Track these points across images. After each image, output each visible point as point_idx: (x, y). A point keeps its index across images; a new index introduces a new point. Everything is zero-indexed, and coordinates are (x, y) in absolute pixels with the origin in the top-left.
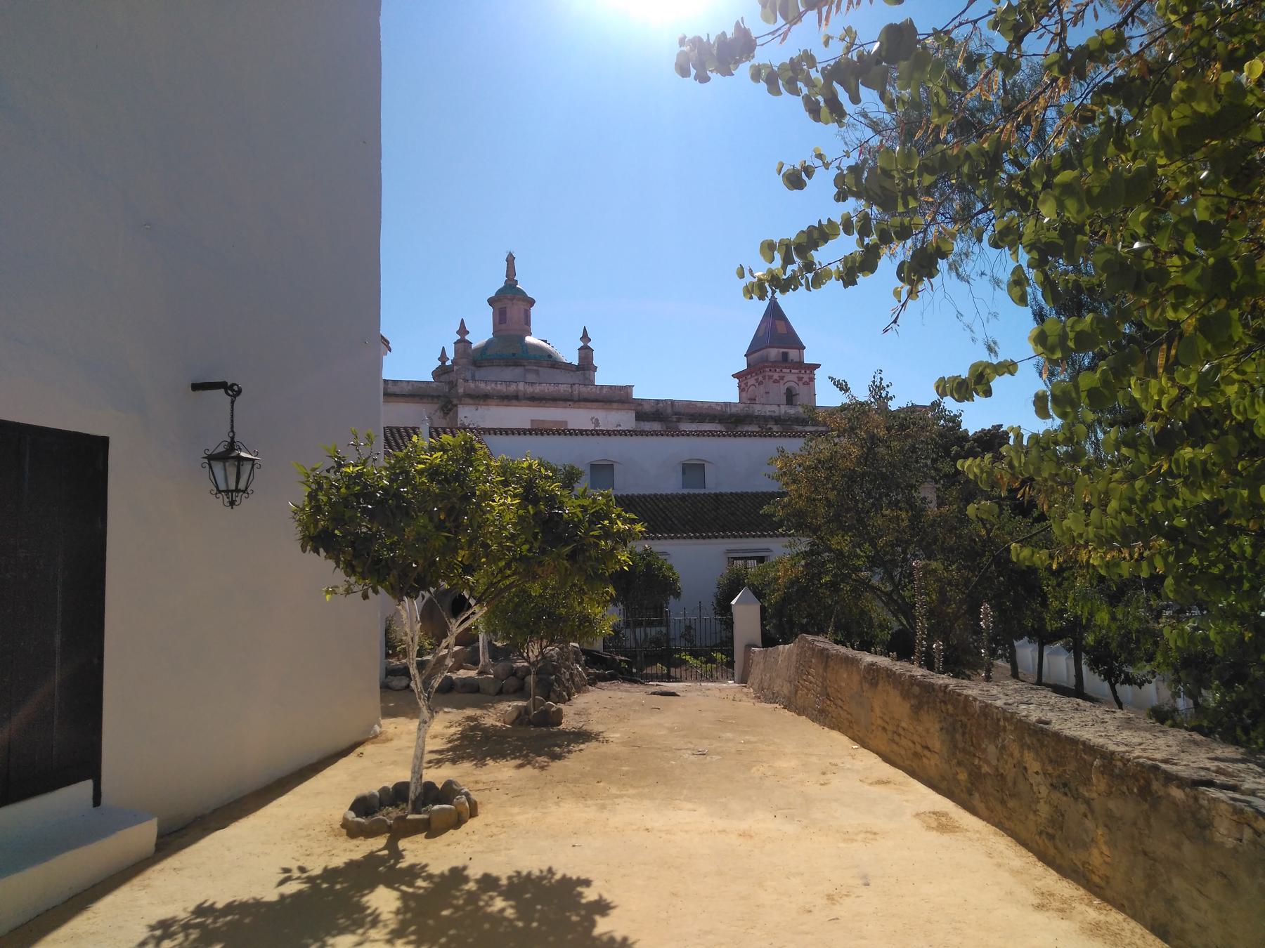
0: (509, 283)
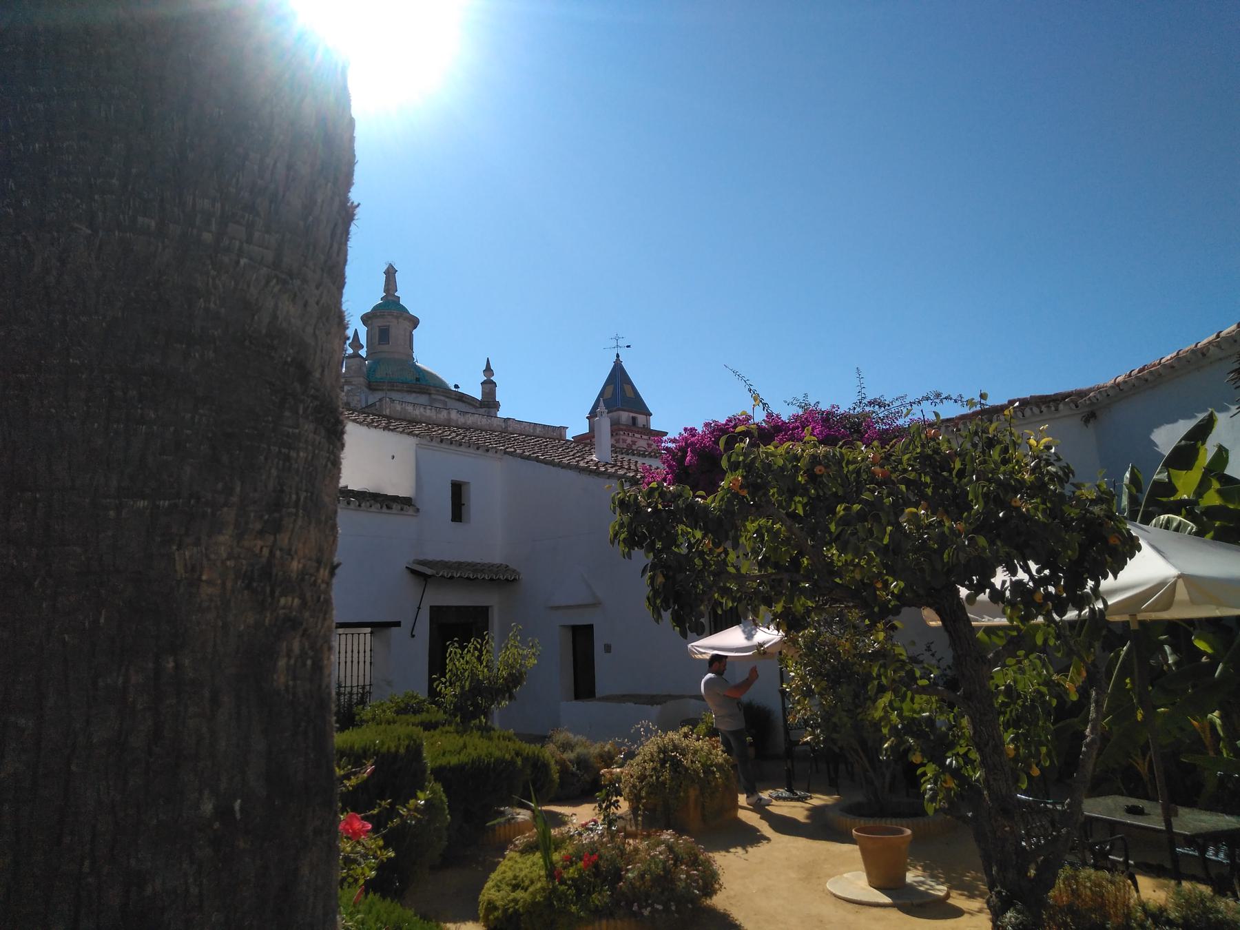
0: (390, 298)
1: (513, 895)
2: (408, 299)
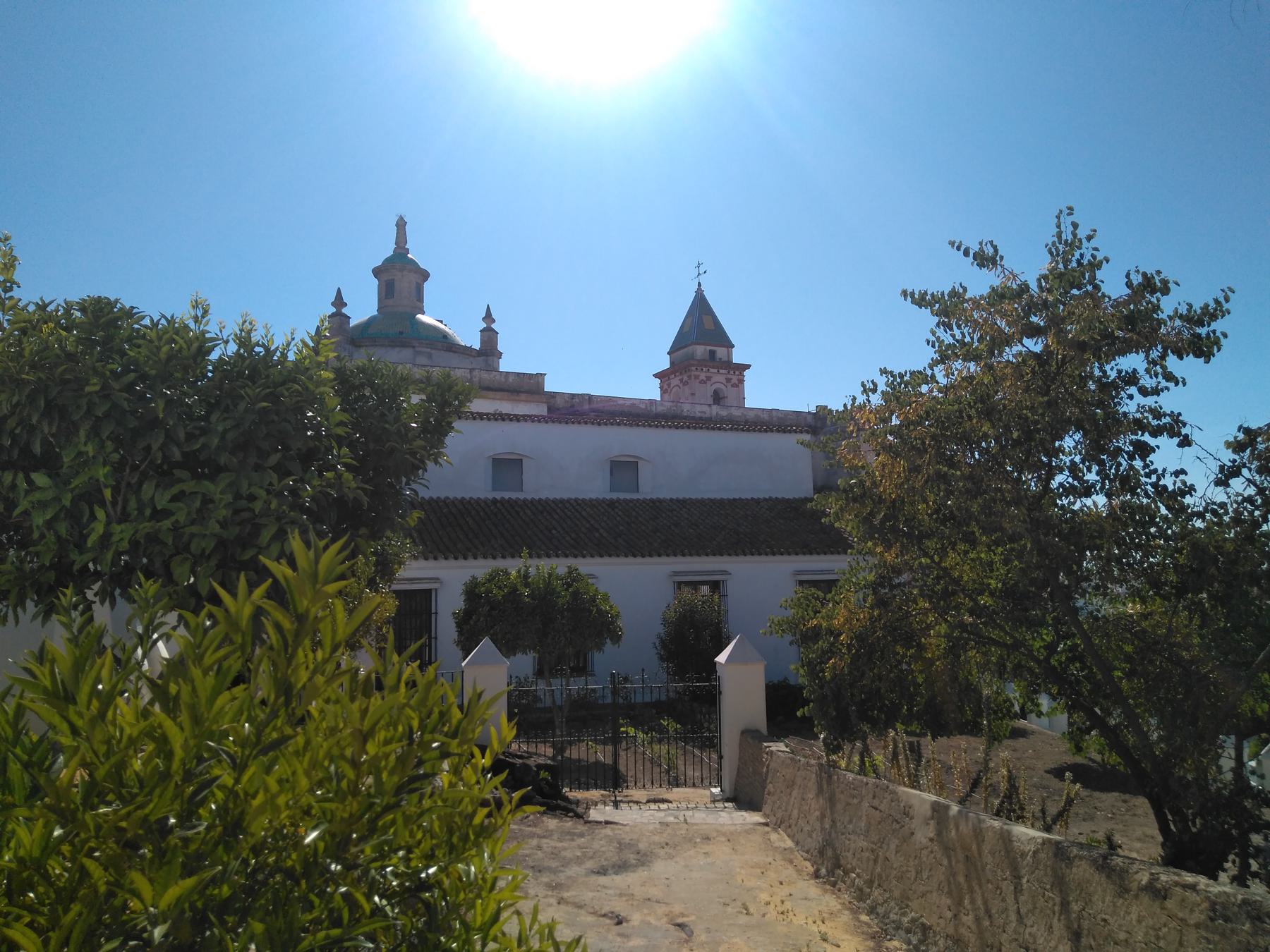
0: (400, 251)
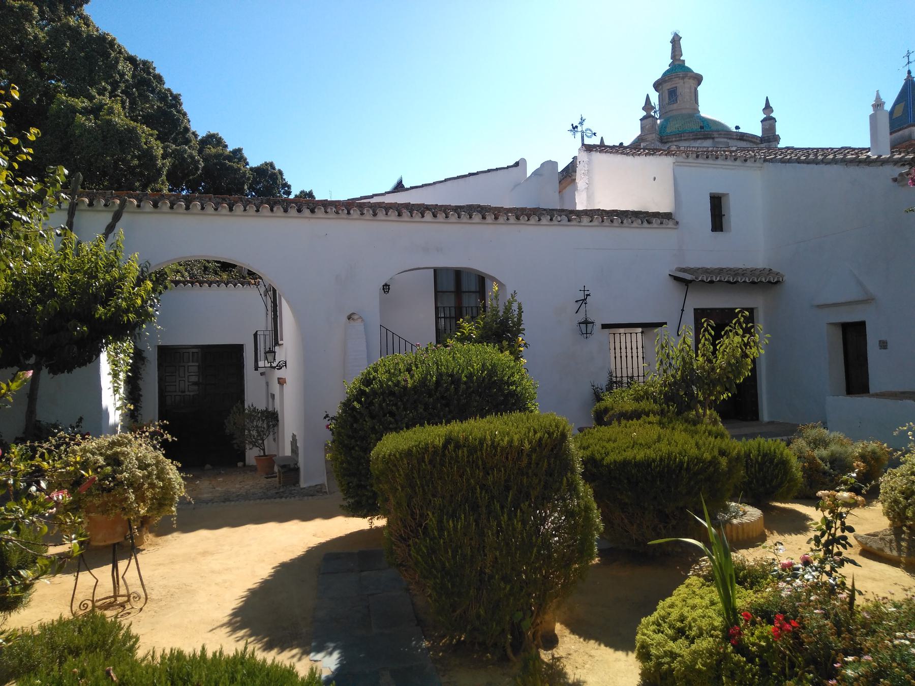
0: (677, 63)
1: (671, 646)
2: (691, 60)
